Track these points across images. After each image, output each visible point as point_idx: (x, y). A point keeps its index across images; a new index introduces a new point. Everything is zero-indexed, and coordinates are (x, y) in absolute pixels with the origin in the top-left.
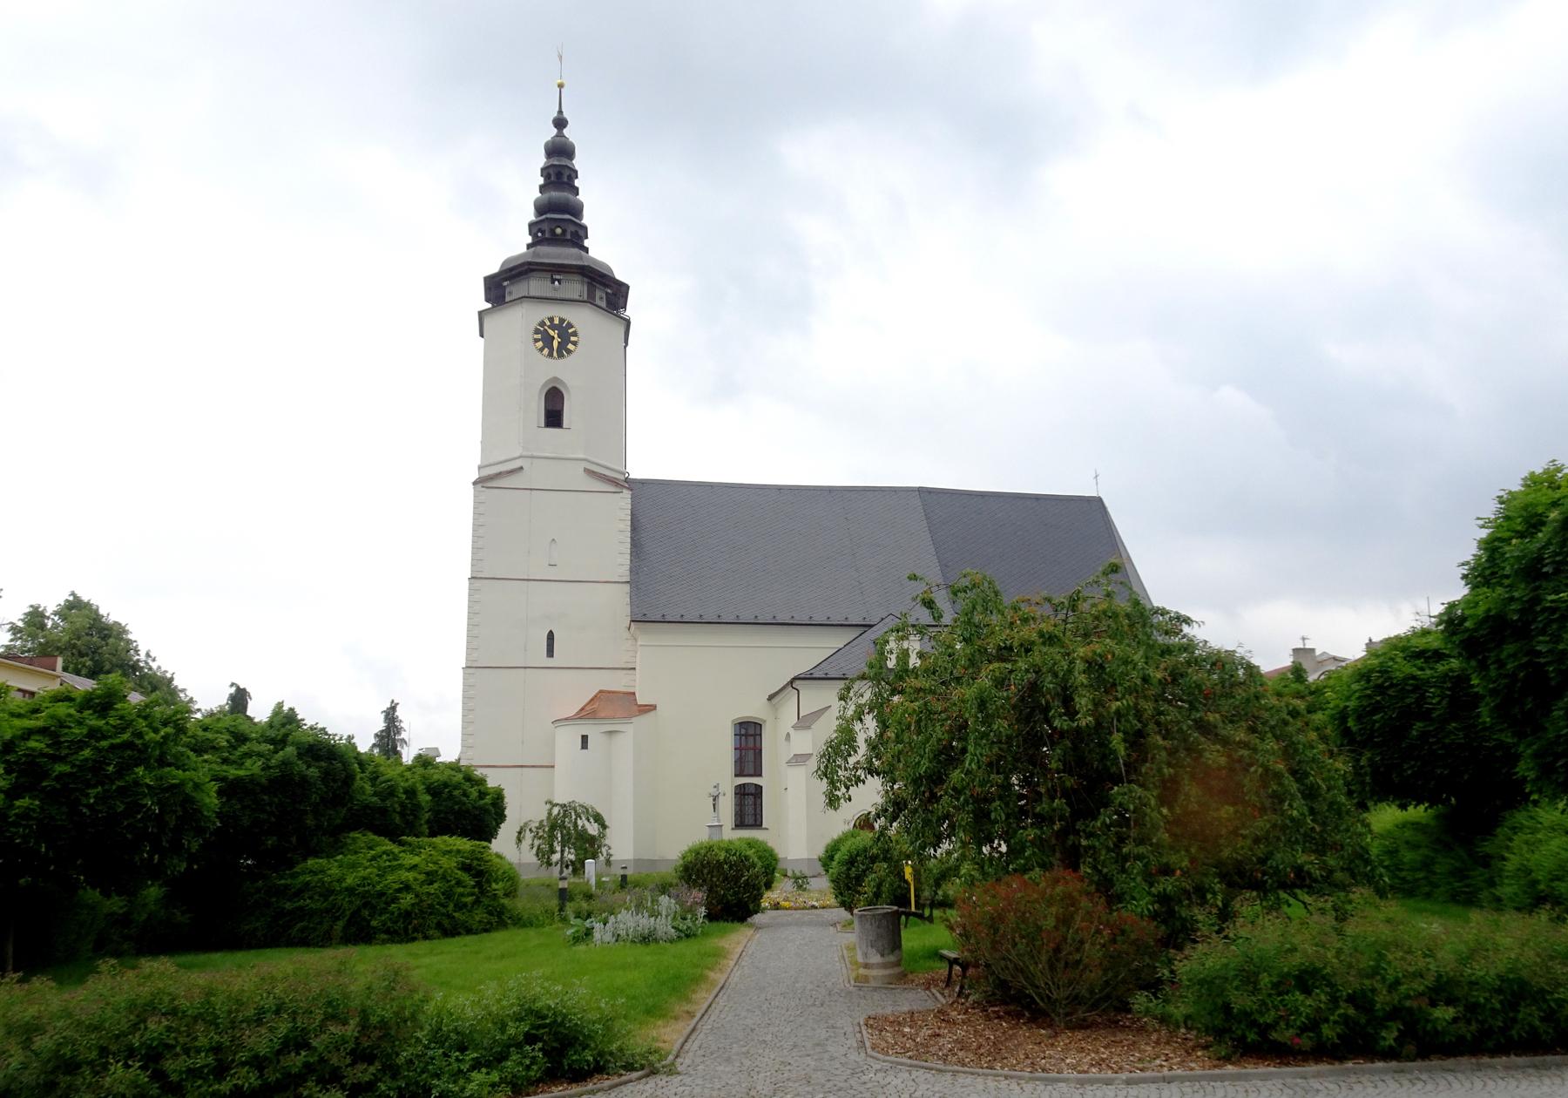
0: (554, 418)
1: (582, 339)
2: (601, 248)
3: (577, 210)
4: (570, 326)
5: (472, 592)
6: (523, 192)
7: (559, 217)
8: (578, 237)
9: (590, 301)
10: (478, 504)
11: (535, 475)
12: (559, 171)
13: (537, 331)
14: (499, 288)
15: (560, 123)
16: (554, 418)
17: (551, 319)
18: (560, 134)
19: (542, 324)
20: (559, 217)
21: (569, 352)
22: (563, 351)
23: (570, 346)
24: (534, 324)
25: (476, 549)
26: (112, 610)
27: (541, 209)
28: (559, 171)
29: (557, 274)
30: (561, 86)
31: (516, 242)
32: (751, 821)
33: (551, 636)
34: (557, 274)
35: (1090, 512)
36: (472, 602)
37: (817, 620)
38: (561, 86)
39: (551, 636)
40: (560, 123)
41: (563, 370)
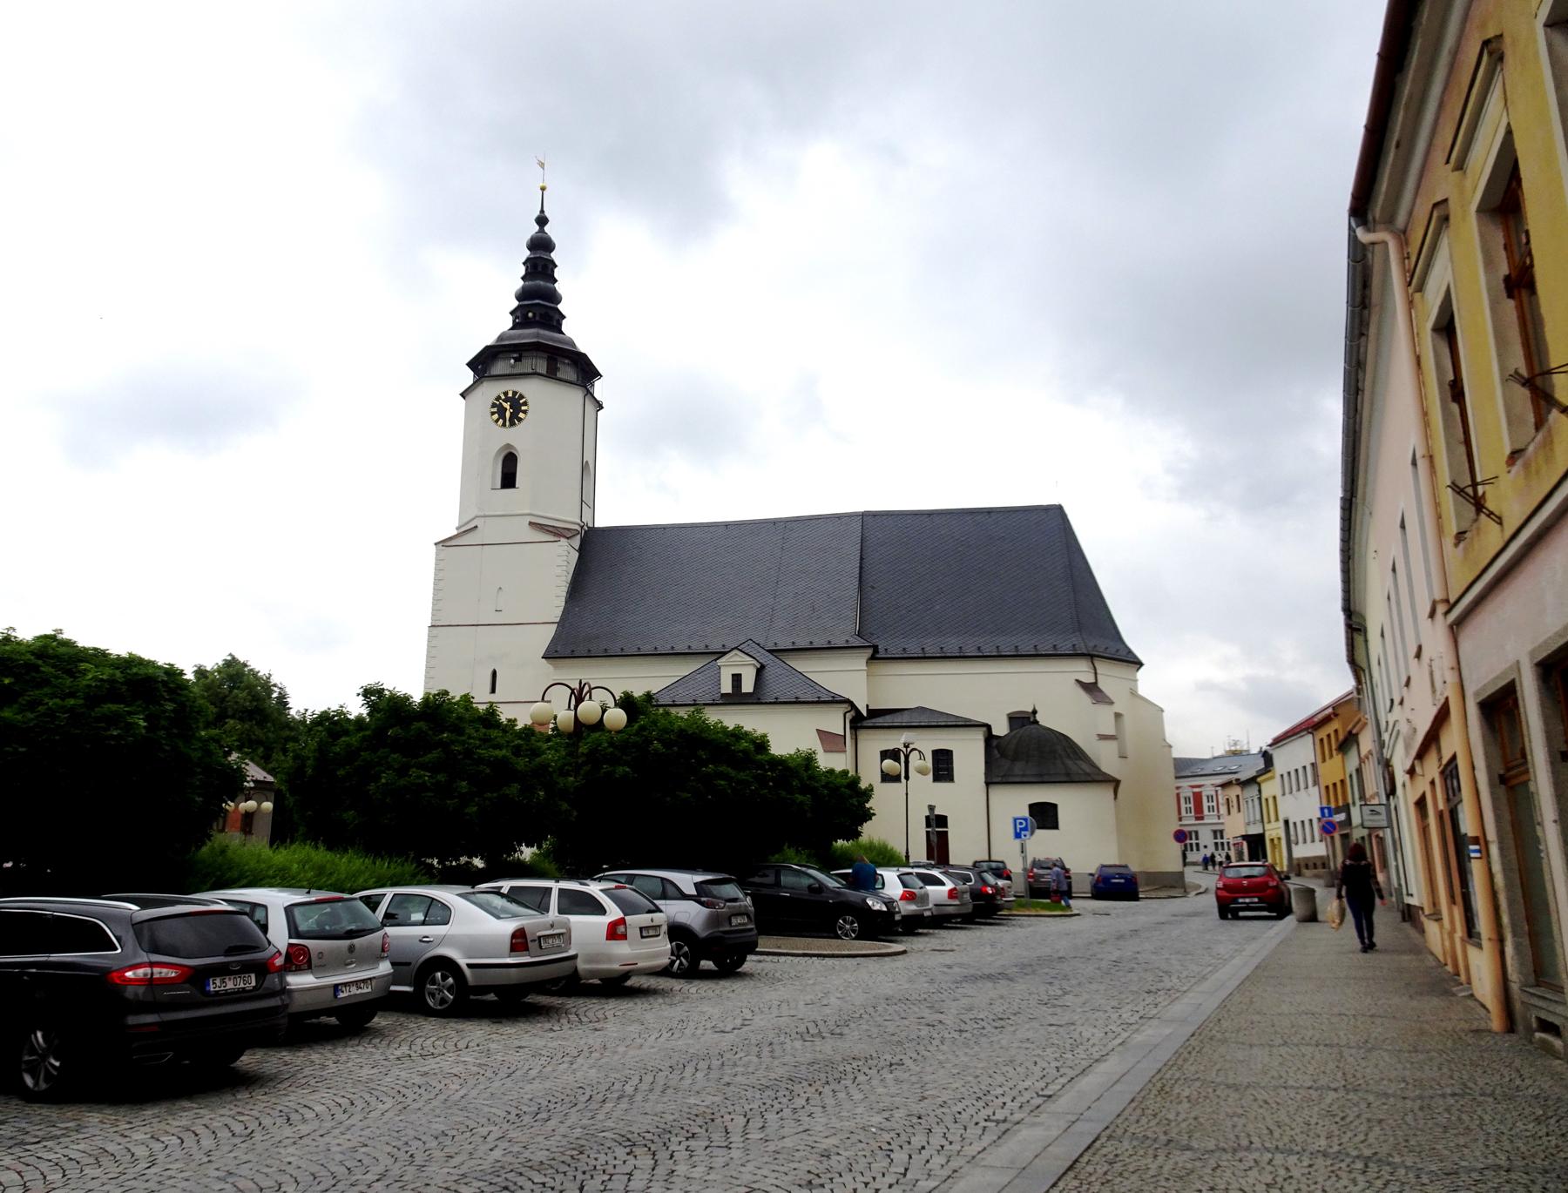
0: (509, 480)
1: (531, 408)
2: (578, 329)
3: (555, 298)
4: (522, 397)
5: (431, 638)
6: (512, 278)
7: (538, 301)
8: (553, 320)
9: (551, 374)
10: (438, 561)
11: (487, 532)
12: (540, 262)
13: (494, 405)
14: (482, 364)
15: (542, 221)
16: (509, 480)
17: (506, 394)
18: (542, 230)
19: (498, 398)
20: (538, 301)
21: (520, 420)
22: (514, 420)
23: (521, 415)
24: (492, 400)
25: (436, 601)
26: (260, 662)
27: (522, 296)
28: (540, 262)
29: (536, 348)
30: (543, 189)
31: (494, 319)
32: (297, 911)
33: (494, 673)
34: (536, 348)
35: (1057, 513)
36: (431, 647)
37: (680, 648)
38: (543, 189)
39: (494, 673)
40: (542, 221)
41: (516, 437)
